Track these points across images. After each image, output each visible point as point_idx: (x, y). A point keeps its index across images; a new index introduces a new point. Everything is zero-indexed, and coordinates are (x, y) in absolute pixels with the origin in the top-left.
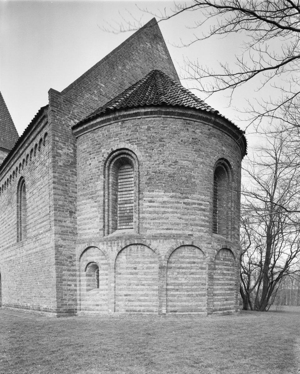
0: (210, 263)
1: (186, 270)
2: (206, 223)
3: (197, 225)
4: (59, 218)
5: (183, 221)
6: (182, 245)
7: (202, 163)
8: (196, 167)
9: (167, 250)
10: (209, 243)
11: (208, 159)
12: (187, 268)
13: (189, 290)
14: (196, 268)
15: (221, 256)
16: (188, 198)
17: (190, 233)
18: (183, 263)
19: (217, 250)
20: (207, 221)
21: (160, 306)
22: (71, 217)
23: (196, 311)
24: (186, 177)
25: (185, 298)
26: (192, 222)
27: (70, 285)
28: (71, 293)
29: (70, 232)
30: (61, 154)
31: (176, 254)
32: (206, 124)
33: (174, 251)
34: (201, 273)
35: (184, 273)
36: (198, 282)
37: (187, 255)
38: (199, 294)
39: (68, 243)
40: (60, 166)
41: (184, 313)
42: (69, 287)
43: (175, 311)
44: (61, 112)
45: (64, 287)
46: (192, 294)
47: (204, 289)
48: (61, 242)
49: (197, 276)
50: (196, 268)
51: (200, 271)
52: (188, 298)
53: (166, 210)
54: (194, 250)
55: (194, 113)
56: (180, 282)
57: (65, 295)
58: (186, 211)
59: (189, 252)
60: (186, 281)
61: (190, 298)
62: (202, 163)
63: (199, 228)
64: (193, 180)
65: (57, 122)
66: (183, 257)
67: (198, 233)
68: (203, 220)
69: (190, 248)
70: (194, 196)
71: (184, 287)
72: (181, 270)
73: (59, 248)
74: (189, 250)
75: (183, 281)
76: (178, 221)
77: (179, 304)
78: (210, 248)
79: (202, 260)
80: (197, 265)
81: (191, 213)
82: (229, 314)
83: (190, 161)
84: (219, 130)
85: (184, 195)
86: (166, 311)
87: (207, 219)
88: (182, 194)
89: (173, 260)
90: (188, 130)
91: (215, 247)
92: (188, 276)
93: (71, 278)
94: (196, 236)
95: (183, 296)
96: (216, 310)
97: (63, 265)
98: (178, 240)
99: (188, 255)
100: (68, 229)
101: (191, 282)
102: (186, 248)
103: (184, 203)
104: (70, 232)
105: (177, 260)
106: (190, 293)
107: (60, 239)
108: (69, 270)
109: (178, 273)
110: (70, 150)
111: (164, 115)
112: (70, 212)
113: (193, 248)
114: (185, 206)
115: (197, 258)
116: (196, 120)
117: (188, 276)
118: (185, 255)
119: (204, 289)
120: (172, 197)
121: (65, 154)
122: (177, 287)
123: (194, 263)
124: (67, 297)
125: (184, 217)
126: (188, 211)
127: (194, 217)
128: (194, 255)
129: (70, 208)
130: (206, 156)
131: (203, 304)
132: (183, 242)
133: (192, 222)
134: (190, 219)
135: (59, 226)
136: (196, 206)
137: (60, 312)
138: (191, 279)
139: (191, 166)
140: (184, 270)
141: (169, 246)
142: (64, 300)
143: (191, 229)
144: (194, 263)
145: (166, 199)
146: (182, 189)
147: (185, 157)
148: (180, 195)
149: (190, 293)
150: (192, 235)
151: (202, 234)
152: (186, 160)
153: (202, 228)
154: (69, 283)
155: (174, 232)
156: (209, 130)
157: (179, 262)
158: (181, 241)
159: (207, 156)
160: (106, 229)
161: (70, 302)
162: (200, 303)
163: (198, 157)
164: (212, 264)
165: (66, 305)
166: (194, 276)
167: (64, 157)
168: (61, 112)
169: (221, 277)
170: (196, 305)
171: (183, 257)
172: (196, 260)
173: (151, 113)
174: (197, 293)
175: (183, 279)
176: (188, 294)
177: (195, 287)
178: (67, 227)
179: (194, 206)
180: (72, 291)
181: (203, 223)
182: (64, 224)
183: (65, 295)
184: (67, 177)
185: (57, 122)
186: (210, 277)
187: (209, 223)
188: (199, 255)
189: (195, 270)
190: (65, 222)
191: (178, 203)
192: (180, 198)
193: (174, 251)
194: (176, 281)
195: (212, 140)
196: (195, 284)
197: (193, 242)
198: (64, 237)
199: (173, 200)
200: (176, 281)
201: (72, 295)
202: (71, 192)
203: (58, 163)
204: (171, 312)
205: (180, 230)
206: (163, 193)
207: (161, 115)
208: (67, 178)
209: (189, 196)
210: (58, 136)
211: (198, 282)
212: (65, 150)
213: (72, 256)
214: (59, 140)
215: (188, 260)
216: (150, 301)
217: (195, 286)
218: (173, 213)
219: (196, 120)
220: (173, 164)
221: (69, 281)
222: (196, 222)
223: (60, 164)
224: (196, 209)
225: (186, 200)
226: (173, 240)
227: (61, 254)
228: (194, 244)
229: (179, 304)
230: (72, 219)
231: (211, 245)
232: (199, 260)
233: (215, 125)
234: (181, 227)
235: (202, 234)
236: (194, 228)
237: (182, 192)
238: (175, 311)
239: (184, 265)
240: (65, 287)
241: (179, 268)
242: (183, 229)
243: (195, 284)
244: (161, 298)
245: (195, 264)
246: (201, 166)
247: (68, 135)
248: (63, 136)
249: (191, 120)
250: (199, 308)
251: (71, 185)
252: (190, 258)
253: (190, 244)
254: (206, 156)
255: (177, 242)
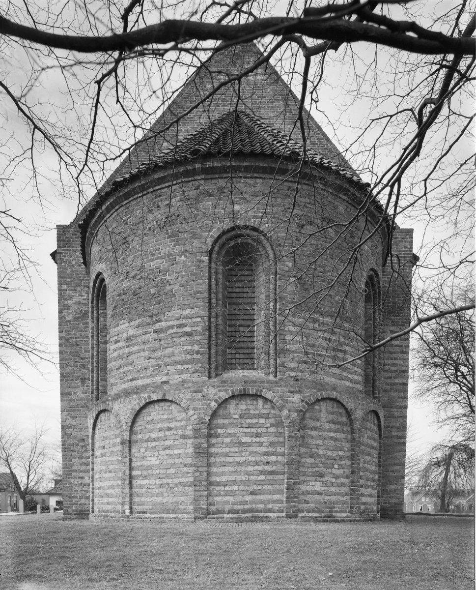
0: (198, 427)
1: (158, 443)
2: (195, 356)
3: (176, 363)
4: (67, 390)
5: (153, 362)
6: (148, 401)
7: (183, 253)
8: (173, 264)
9: (128, 413)
10: (195, 392)
11: (195, 241)
12: (158, 439)
13: (162, 476)
14: (173, 437)
15: (232, 411)
16: (161, 321)
17: (164, 379)
18: (152, 431)
19: (216, 401)
20: (198, 353)
21: (123, 504)
22: (83, 386)
23: (175, 511)
24: (156, 286)
25: (157, 490)
26: (168, 360)
27: (82, 478)
28: (84, 489)
29: (82, 407)
30: (70, 305)
31: (142, 418)
32: (189, 182)
33: (138, 414)
34: (183, 445)
35: (155, 448)
36: (177, 461)
37: (157, 417)
38: (180, 483)
39: (78, 422)
40: (69, 321)
41: (156, 516)
42: (80, 481)
43: (144, 513)
44: (70, 250)
45: (73, 480)
46: (168, 484)
47: (188, 473)
48: (70, 421)
49: (177, 452)
50: (173, 437)
51: (182, 441)
52: (161, 490)
53: (131, 350)
54: (169, 406)
55: (161, 174)
56: (149, 463)
57: (75, 491)
58: (157, 344)
59: (161, 412)
60: (157, 462)
61: (164, 490)
62: (183, 253)
63: (180, 367)
64: (168, 288)
65: (65, 266)
66: (151, 422)
67: (177, 377)
68: (188, 352)
69: (162, 404)
70: (170, 314)
71: (155, 472)
72: (150, 444)
73: (67, 430)
74: (160, 409)
75: (154, 461)
76: (146, 363)
77: (148, 499)
78: (198, 400)
79: (184, 423)
80: (176, 433)
81: (166, 345)
82: (329, 519)
83: (161, 258)
84: (222, 178)
85: (155, 318)
86: (129, 511)
87: (196, 348)
88: (151, 317)
89: (139, 428)
90: (158, 207)
91: (212, 396)
92: (160, 452)
93: (83, 468)
94: (175, 381)
95: (154, 487)
96: (218, 512)
97: (72, 451)
98: (142, 395)
99: (159, 417)
100: (79, 402)
101: (165, 462)
102: (157, 407)
103: (155, 331)
104: (82, 407)
105: (143, 427)
106: (164, 481)
107: (68, 417)
108: (81, 458)
109: (146, 449)
110: (82, 296)
111: (126, 200)
112: (82, 379)
113: (168, 404)
114: (155, 335)
115: (174, 419)
116: (170, 183)
117: (160, 452)
118: (155, 418)
119: (188, 473)
120: (138, 326)
121: (76, 303)
122: (145, 473)
123: (170, 429)
124: (78, 494)
125: (154, 355)
126: (161, 343)
127: (171, 349)
128: (171, 416)
129: (82, 374)
130: (192, 238)
131: (186, 501)
132: (149, 397)
133: (167, 360)
134: (164, 355)
135: (67, 400)
136: (175, 330)
137: (68, 514)
138: (166, 457)
139: (164, 264)
140: (154, 444)
141: (130, 407)
142: (73, 497)
143: (166, 372)
144: (170, 429)
145: (131, 332)
146: (151, 308)
147: (154, 254)
148: (149, 320)
149: (164, 481)
150: (167, 382)
151: (186, 376)
152: (157, 258)
153: (186, 366)
154: (81, 475)
155: (140, 383)
156: (197, 188)
157: (147, 431)
158: (146, 395)
159: (195, 236)
160: (95, 394)
161: (83, 501)
162: (182, 499)
163: (175, 245)
164: (203, 427)
165: (77, 504)
166: (171, 452)
167: (74, 308)
168: (70, 250)
169: (236, 449)
170: (176, 502)
171: (151, 422)
172: (173, 424)
173: (112, 206)
174: (176, 481)
175: (153, 458)
176: (161, 483)
177: (172, 471)
178: (78, 400)
179: (170, 331)
180: (85, 485)
181: (189, 357)
182: (73, 397)
183: (75, 491)
184: (78, 333)
185: (65, 266)
186: (197, 451)
187: (201, 354)
188: (178, 415)
189: (172, 441)
190: (75, 393)
191: (146, 333)
192: (149, 324)
193: (138, 414)
194: (144, 463)
195: (204, 204)
196: (172, 466)
197: (164, 395)
198: (73, 414)
199: (140, 331)
200: (144, 463)
201: (85, 491)
202: (83, 352)
203: (65, 318)
204: (139, 513)
205: (148, 377)
206: (127, 325)
207: (123, 202)
208: (78, 334)
209: (161, 317)
210: (65, 284)
211: (177, 461)
212: (77, 299)
213: (85, 438)
214: (68, 287)
215: (159, 426)
216: (116, 497)
217: (172, 469)
218: (139, 351)
219: (170, 183)
220: (138, 272)
221: (81, 471)
222: (174, 359)
223: (68, 318)
224: (174, 335)
225: (157, 326)
226: (135, 396)
227: (69, 437)
228: (167, 398)
229: (148, 499)
230: (85, 388)
231: (200, 394)
232: (178, 424)
233: (207, 174)
234: (149, 372)
235: (186, 376)
236: (171, 369)
237: (151, 314)
238: (144, 513)
239: (154, 435)
240: (76, 481)
241: (147, 441)
242: (153, 375)
243: (172, 466)
244: (124, 491)
245: (173, 431)
246: (183, 258)
247: (80, 277)
248: (72, 281)
249: (163, 188)
250: (180, 507)
251: (83, 342)
252: (161, 421)
253: (160, 397)
254: (192, 238)
255: (140, 399)
